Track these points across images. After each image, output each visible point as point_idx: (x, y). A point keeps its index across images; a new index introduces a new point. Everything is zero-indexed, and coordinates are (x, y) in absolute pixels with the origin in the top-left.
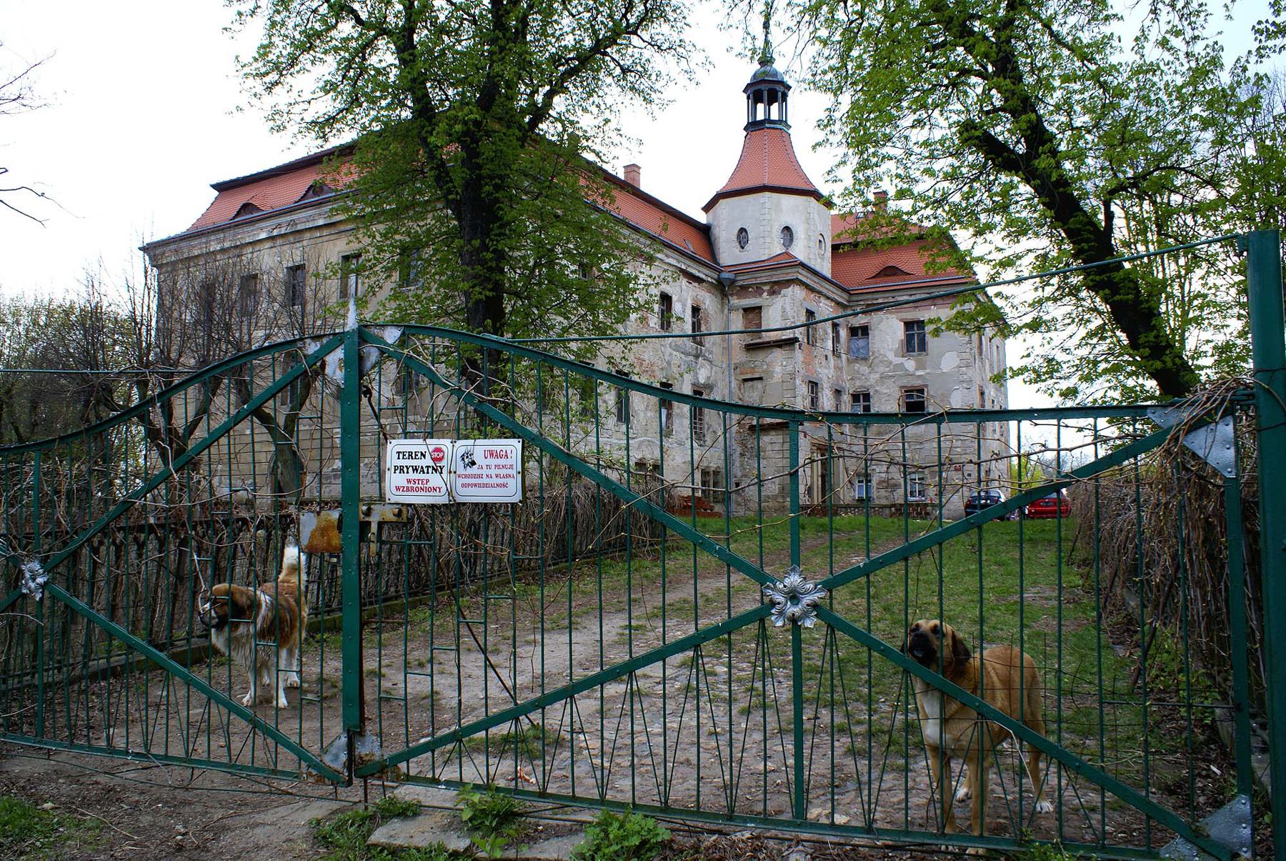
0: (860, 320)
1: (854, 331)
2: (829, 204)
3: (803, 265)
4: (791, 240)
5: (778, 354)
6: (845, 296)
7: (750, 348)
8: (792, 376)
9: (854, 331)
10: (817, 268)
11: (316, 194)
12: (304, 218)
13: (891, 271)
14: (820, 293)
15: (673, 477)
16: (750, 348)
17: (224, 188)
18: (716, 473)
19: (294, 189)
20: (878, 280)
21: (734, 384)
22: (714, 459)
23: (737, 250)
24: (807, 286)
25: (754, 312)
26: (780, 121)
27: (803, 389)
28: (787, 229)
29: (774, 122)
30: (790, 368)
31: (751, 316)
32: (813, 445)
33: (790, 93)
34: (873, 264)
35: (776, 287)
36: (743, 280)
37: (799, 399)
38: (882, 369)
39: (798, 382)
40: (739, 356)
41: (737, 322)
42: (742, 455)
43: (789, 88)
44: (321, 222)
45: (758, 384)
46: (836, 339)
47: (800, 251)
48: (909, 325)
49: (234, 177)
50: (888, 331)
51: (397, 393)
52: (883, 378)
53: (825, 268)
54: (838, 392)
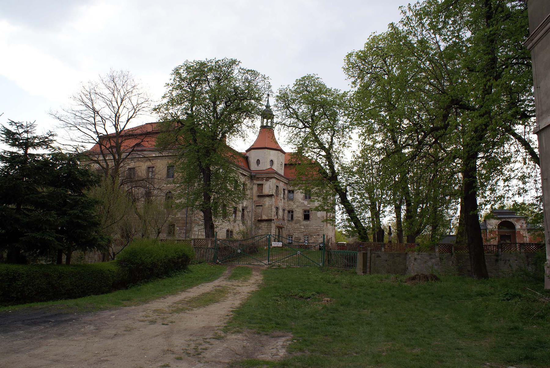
0: (291, 188)
5: (267, 199)
7: (259, 196)
16: (259, 196)
21: (253, 207)
23: (256, 166)
24: (277, 179)
25: (260, 186)
28: (272, 160)
30: (271, 203)
35: (268, 179)
36: (258, 176)
40: (255, 198)
41: (255, 188)
42: (255, 229)
45: (261, 207)
47: (275, 167)
54: (284, 210)
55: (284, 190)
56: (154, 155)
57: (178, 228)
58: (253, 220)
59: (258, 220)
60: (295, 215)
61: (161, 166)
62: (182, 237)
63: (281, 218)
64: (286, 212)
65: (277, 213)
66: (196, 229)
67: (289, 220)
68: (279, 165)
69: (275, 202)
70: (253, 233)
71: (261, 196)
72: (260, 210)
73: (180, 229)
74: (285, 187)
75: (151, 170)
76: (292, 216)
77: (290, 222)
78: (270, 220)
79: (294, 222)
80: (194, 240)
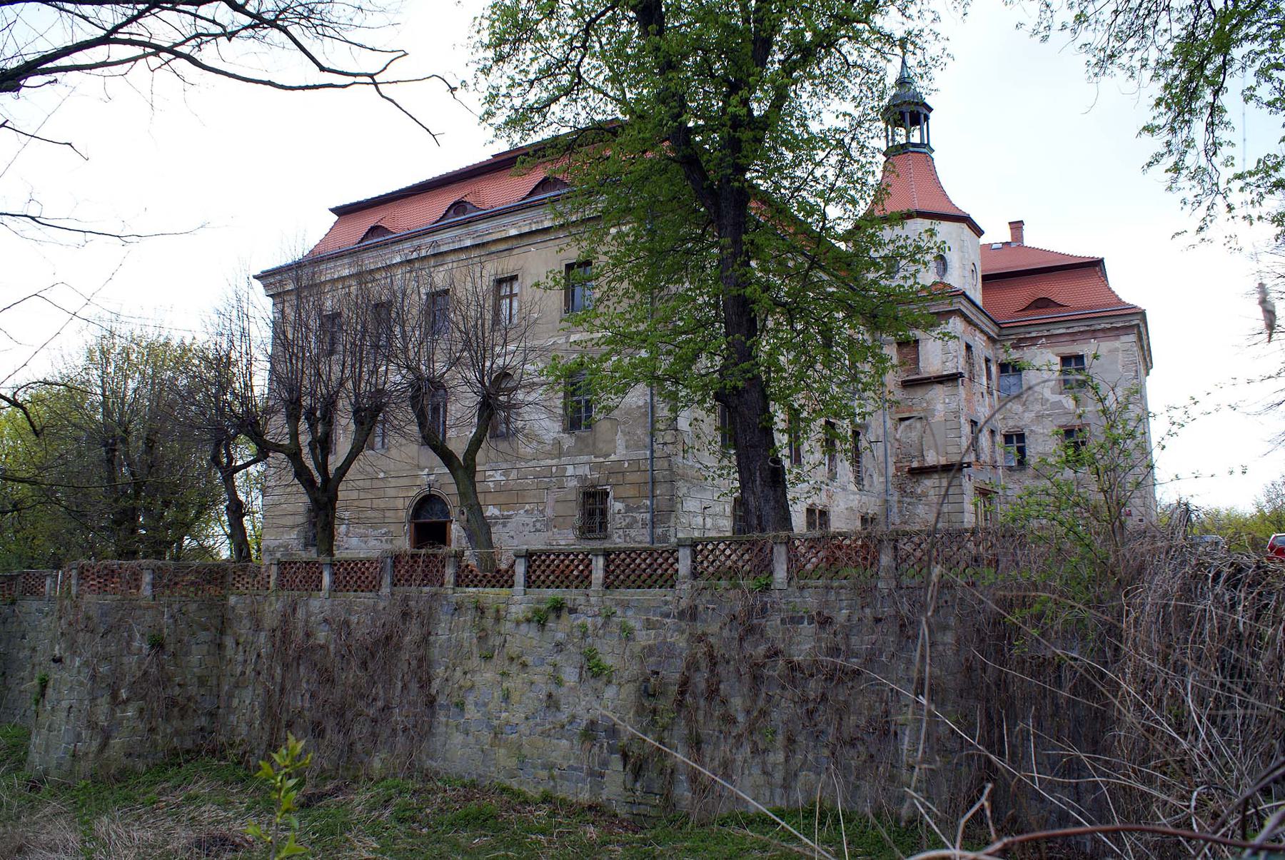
1: (1004, 368)
2: (979, 232)
3: (964, 294)
4: (945, 270)
5: (939, 392)
6: (996, 330)
7: (906, 385)
8: (957, 413)
9: (1004, 368)
10: (972, 297)
11: (457, 214)
12: (447, 240)
13: (1043, 303)
14: (976, 325)
15: (838, 525)
16: (906, 385)
17: (343, 212)
18: (873, 519)
19: (438, 205)
20: (1029, 312)
21: (889, 423)
22: (873, 508)
25: (909, 346)
26: (921, 145)
27: (967, 429)
29: (914, 145)
30: (953, 406)
31: (905, 350)
32: (976, 488)
33: (931, 115)
34: (1022, 294)
37: (964, 439)
38: (1038, 407)
39: (963, 420)
43: (930, 110)
44: (468, 243)
46: (988, 369)
48: (1066, 360)
49: (354, 200)
50: (1043, 361)
51: (564, 431)
52: (1039, 417)
53: (977, 296)
55: (987, 360)
56: (513, 232)
57: (619, 506)
58: (891, 470)
59: (913, 472)
60: (1035, 449)
61: (540, 264)
62: (640, 537)
63: (988, 460)
64: (999, 439)
65: (975, 441)
66: (691, 505)
67: (1010, 468)
68: (968, 274)
69: (969, 401)
70: (895, 518)
71: (914, 384)
72: (914, 435)
73: (629, 509)
74: (989, 353)
75: (505, 290)
76: (1021, 451)
77: (1017, 476)
78: (951, 469)
79: (1030, 471)
80: (693, 544)
